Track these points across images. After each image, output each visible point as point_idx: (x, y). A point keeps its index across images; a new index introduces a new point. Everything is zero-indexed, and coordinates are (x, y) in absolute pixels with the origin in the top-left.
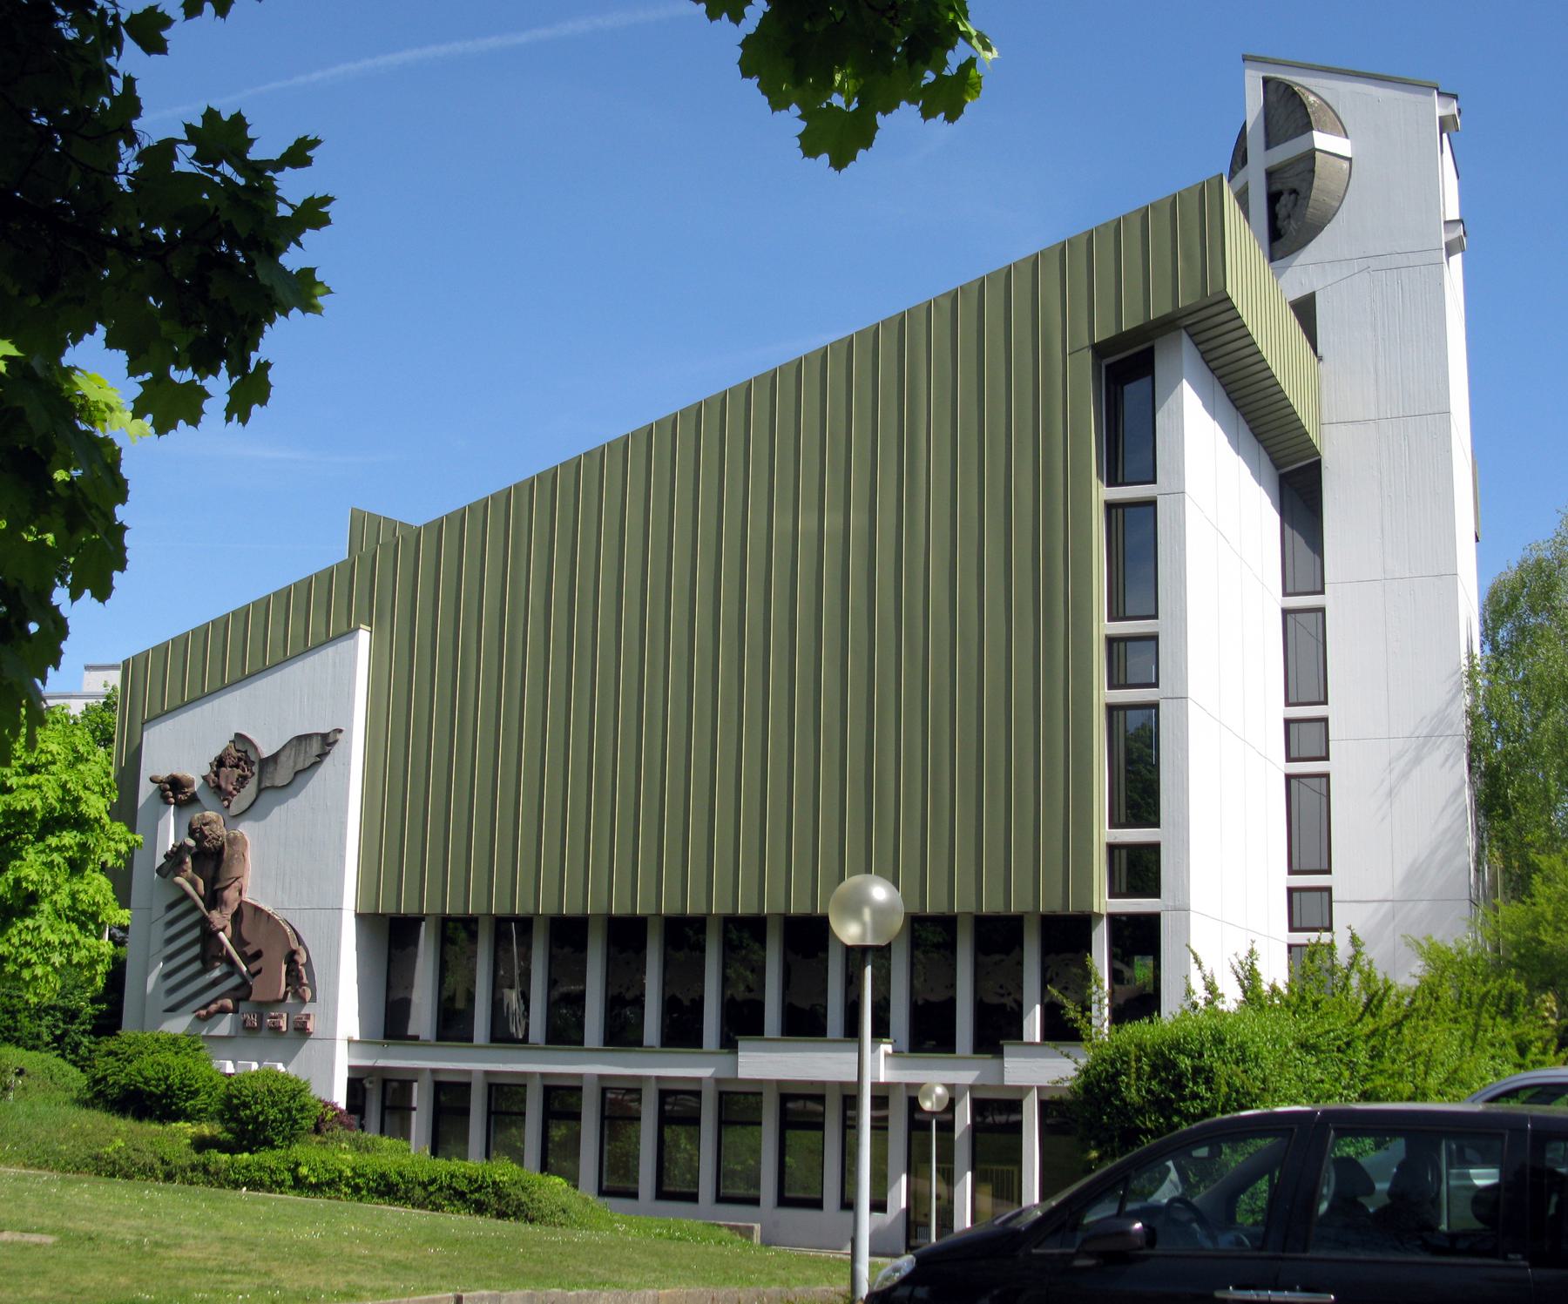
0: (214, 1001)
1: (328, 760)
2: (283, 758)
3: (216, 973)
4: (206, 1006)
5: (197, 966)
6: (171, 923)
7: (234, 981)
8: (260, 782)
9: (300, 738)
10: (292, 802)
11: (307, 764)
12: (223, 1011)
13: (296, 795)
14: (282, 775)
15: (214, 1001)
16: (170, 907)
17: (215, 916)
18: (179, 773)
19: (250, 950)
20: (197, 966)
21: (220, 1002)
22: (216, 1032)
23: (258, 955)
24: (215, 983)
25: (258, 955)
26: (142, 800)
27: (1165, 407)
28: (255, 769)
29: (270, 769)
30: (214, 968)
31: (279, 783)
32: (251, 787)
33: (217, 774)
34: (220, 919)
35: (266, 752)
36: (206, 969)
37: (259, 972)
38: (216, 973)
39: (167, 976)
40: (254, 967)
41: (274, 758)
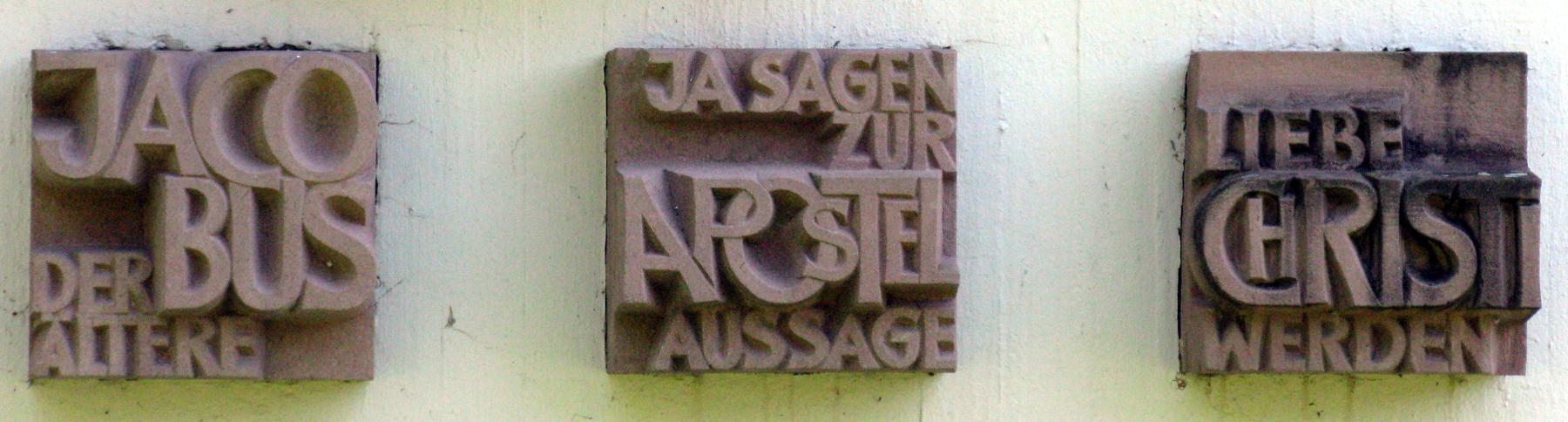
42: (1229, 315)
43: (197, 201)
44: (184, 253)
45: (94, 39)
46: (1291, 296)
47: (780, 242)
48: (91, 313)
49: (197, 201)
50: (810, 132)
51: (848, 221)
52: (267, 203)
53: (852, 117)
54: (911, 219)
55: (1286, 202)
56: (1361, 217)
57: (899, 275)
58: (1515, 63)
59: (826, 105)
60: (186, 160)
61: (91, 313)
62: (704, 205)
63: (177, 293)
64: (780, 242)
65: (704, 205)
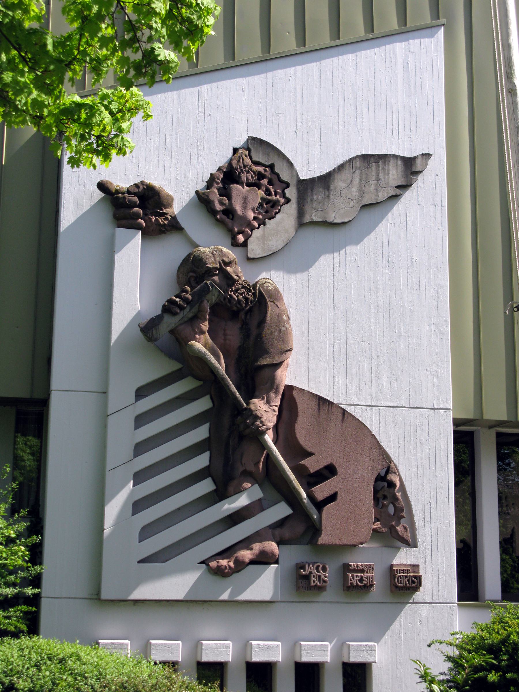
0: (246, 543)
1: (409, 195)
2: (339, 183)
3: (242, 501)
4: (227, 552)
5: (206, 486)
6: (141, 420)
7: (281, 510)
8: (301, 213)
9: (367, 159)
10: (351, 250)
11: (382, 196)
12: (264, 559)
13: (357, 241)
14: (339, 207)
15: (246, 543)
16: (141, 393)
17: (259, 405)
18: (156, 182)
19: (313, 465)
20: (206, 486)
21: (257, 547)
22: (246, 596)
23: (330, 471)
24: (235, 519)
25: (330, 471)
26: (68, 216)
27: (124, 250)
28: (291, 193)
29: (319, 195)
30: (239, 491)
31: (334, 217)
32: (286, 217)
33: (225, 193)
34: (266, 411)
35: (305, 173)
36: (220, 494)
37: (333, 498)
38: (242, 501)
39: (138, 506)
40: (321, 491)
41: (325, 180)
42: (397, 587)
43: (314, 576)
44: (313, 451)
45: (59, 36)
46: (402, 585)
47: (361, 580)
48: (305, 585)
49: (314, 576)
50: (362, 571)
51: (367, 578)
52: (320, 576)
53: (366, 569)
54: (372, 578)
55: (353, 578)
56: (408, 578)
57: (371, 583)
58: (419, 565)
59: (35, 638)
60: (313, 572)
61: (305, 585)
62: (355, 577)
63: (313, 584)
64: (361, 580)
65: (355, 577)
